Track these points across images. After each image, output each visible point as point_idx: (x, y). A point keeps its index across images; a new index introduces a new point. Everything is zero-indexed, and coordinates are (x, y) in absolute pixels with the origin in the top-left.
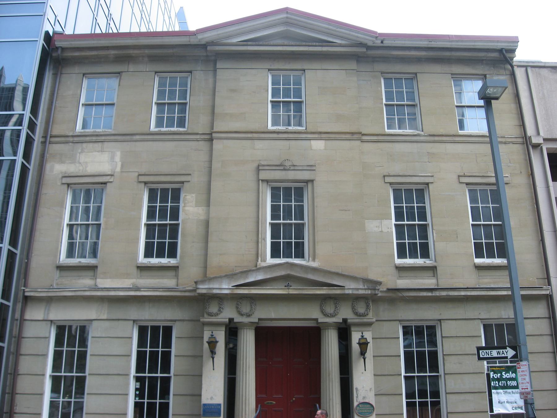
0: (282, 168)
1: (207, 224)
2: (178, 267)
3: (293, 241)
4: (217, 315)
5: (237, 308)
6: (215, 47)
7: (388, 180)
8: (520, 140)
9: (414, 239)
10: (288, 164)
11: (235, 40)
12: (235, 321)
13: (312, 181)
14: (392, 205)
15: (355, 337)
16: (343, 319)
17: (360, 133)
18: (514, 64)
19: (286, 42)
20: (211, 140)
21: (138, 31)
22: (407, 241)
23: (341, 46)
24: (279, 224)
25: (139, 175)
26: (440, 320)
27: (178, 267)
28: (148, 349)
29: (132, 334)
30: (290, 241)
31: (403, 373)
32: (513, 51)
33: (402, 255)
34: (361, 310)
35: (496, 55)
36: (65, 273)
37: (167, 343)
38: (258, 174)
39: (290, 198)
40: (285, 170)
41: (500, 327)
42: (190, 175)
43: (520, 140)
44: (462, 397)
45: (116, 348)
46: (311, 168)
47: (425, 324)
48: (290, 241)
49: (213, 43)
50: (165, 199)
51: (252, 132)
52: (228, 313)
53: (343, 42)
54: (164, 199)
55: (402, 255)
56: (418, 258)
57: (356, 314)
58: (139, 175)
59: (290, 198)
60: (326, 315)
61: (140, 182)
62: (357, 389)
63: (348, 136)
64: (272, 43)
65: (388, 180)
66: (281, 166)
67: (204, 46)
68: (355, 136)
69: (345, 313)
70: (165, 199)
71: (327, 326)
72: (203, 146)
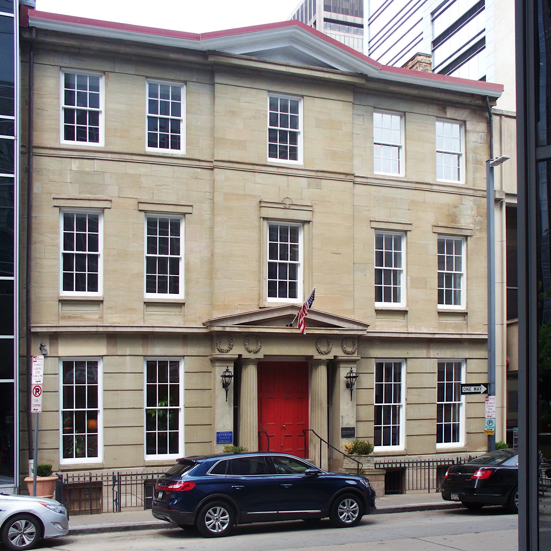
0: (282, 206)
1: (211, 260)
2: (467, 313)
3: (87, 273)
4: (228, 351)
6: (218, 57)
7: (142, 207)
8: (35, 151)
9: (385, 285)
10: (288, 202)
11: (237, 52)
14: (62, 232)
15: (343, 372)
16: (239, 355)
18: (492, 111)
19: (293, 63)
22: (75, 272)
23: (343, 74)
25: (139, 203)
26: (406, 359)
27: (467, 313)
28: (157, 384)
29: (143, 369)
30: (281, 279)
31: (61, 409)
32: (494, 99)
33: (68, 286)
35: (479, 102)
36: (151, 309)
37: (175, 377)
39: (283, 237)
42: (192, 206)
43: (35, 151)
44: (418, 422)
45: (417, 381)
46: (309, 208)
47: (168, 359)
48: (281, 279)
49: (214, 53)
50: (163, 233)
52: (238, 350)
53: (342, 69)
54: (81, 227)
55: (68, 286)
57: (345, 352)
58: (139, 203)
59: (283, 237)
60: (321, 353)
61: (140, 210)
62: (342, 416)
63: (342, 177)
64: (272, 60)
66: (282, 205)
67: (205, 54)
68: (349, 177)
69: (336, 351)
70: (163, 233)
71: (319, 362)
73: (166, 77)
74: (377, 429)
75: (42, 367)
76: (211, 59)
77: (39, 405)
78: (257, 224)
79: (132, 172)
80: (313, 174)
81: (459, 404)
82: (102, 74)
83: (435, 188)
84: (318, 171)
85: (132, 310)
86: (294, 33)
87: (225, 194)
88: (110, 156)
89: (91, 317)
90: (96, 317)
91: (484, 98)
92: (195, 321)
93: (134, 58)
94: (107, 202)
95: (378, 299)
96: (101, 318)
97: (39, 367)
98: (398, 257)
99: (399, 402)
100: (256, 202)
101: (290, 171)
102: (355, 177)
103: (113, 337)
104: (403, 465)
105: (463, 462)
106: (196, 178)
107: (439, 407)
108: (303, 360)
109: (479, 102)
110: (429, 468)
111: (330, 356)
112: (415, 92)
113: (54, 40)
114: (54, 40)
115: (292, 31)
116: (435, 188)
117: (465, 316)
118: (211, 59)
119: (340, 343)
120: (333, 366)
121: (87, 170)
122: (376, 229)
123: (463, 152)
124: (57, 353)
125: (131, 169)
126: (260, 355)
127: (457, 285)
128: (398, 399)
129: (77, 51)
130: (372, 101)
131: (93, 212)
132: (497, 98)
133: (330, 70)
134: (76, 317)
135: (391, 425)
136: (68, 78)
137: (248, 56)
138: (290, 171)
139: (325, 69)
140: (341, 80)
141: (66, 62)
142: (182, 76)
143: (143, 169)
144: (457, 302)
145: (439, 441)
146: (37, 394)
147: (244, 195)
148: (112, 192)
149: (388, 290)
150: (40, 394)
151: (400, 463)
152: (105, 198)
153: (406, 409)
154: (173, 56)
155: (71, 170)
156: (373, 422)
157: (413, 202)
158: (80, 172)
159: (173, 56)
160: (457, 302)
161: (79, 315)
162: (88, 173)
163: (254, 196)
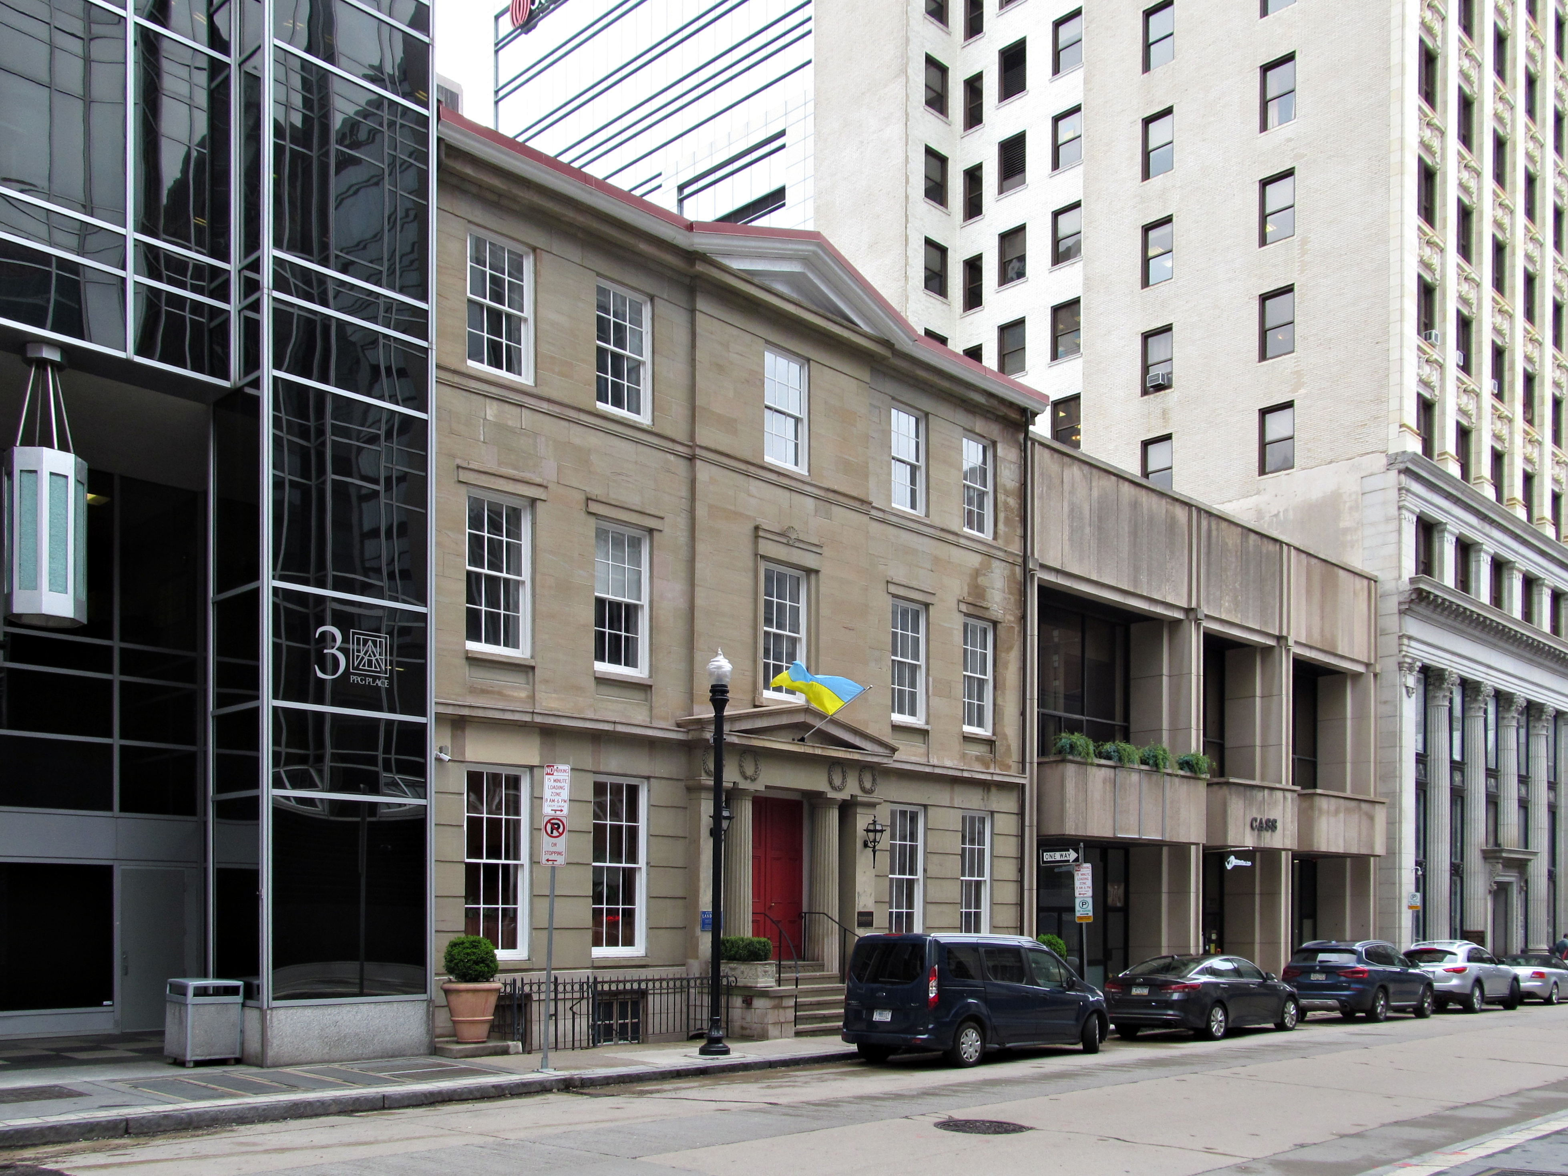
0: (785, 541)
5: (741, 766)
7: (892, 589)
12: (740, 787)
13: (817, 572)
15: (862, 821)
17: (870, 503)
19: (805, 303)
20: (691, 459)
21: (492, 126)
24: (479, 575)
27: (651, 687)
34: (868, 785)
36: (604, 690)
38: (756, 543)
40: (788, 544)
41: (972, 819)
42: (662, 518)
46: (815, 548)
47: (504, 771)
51: (580, 410)
56: (480, 641)
63: (857, 504)
65: (464, 476)
67: (692, 256)
68: (865, 507)
69: (851, 789)
72: (681, 466)
73: (626, 282)
74: (597, 913)
75: (567, 786)
76: (700, 267)
77: (560, 853)
78: (751, 564)
79: (577, 441)
80: (821, 493)
81: (516, 866)
82: (530, 251)
83: (962, 541)
84: (828, 490)
85: (578, 689)
86: (814, 253)
87: (710, 506)
88: (545, 406)
89: (516, 694)
90: (523, 694)
91: (1023, 411)
92: (665, 719)
93: (580, 235)
94: (542, 489)
95: (473, 633)
96: (533, 697)
97: (559, 784)
98: (514, 551)
99: (517, 857)
100: (751, 526)
101: (793, 484)
102: (874, 508)
103: (551, 734)
104: (643, 986)
105: (527, 989)
106: (668, 471)
107: (472, 870)
108: (796, 797)
109: (1014, 415)
110: (556, 1000)
111: (844, 795)
112: (946, 384)
113: (469, 171)
114: (469, 171)
115: (811, 248)
116: (962, 541)
117: (527, 673)
118: (700, 267)
119: (857, 775)
120: (847, 809)
121: (510, 423)
122: (894, 596)
123: (804, 416)
124: (464, 754)
125: (578, 436)
126: (759, 786)
127: (512, 604)
128: (514, 851)
129: (495, 198)
130: (891, 387)
131: (516, 503)
132: (1036, 414)
133: (845, 323)
134: (492, 692)
135: (500, 906)
136: (479, 244)
137: (747, 277)
138: (793, 484)
139: (839, 319)
140: (819, 326)
141: (478, 214)
142: (648, 284)
143: (594, 440)
144: (511, 641)
145: (597, 943)
146: (555, 833)
147: (735, 513)
148: (548, 471)
149: (493, 618)
150: (561, 834)
151: (640, 982)
152: (538, 480)
153: (531, 872)
154: (643, 247)
155: (485, 419)
156: (591, 900)
157: (936, 560)
158: (500, 427)
159: (643, 247)
160: (511, 641)
161: (496, 689)
162: (512, 430)
163: (748, 517)
